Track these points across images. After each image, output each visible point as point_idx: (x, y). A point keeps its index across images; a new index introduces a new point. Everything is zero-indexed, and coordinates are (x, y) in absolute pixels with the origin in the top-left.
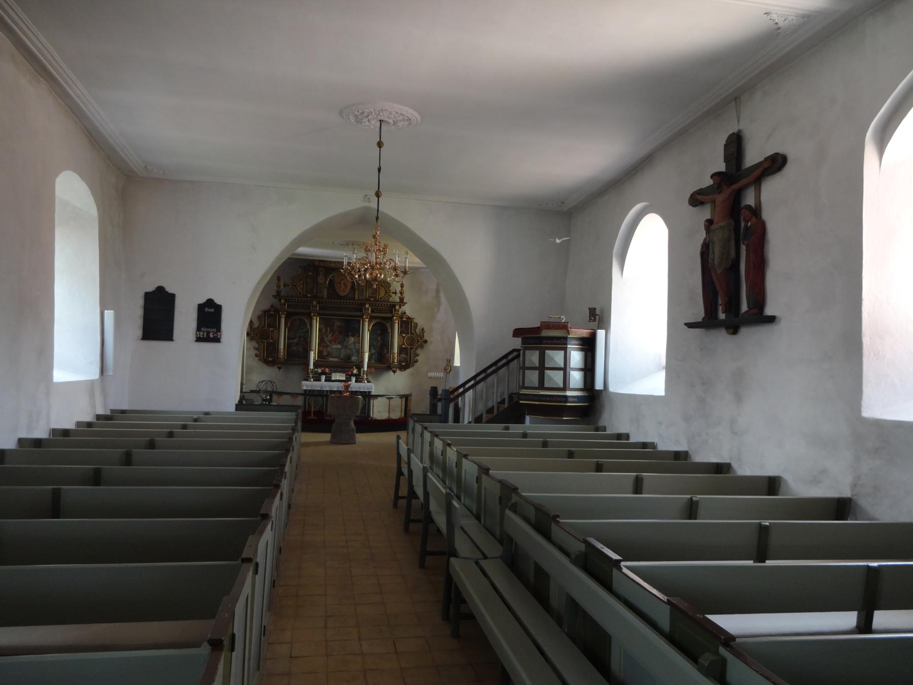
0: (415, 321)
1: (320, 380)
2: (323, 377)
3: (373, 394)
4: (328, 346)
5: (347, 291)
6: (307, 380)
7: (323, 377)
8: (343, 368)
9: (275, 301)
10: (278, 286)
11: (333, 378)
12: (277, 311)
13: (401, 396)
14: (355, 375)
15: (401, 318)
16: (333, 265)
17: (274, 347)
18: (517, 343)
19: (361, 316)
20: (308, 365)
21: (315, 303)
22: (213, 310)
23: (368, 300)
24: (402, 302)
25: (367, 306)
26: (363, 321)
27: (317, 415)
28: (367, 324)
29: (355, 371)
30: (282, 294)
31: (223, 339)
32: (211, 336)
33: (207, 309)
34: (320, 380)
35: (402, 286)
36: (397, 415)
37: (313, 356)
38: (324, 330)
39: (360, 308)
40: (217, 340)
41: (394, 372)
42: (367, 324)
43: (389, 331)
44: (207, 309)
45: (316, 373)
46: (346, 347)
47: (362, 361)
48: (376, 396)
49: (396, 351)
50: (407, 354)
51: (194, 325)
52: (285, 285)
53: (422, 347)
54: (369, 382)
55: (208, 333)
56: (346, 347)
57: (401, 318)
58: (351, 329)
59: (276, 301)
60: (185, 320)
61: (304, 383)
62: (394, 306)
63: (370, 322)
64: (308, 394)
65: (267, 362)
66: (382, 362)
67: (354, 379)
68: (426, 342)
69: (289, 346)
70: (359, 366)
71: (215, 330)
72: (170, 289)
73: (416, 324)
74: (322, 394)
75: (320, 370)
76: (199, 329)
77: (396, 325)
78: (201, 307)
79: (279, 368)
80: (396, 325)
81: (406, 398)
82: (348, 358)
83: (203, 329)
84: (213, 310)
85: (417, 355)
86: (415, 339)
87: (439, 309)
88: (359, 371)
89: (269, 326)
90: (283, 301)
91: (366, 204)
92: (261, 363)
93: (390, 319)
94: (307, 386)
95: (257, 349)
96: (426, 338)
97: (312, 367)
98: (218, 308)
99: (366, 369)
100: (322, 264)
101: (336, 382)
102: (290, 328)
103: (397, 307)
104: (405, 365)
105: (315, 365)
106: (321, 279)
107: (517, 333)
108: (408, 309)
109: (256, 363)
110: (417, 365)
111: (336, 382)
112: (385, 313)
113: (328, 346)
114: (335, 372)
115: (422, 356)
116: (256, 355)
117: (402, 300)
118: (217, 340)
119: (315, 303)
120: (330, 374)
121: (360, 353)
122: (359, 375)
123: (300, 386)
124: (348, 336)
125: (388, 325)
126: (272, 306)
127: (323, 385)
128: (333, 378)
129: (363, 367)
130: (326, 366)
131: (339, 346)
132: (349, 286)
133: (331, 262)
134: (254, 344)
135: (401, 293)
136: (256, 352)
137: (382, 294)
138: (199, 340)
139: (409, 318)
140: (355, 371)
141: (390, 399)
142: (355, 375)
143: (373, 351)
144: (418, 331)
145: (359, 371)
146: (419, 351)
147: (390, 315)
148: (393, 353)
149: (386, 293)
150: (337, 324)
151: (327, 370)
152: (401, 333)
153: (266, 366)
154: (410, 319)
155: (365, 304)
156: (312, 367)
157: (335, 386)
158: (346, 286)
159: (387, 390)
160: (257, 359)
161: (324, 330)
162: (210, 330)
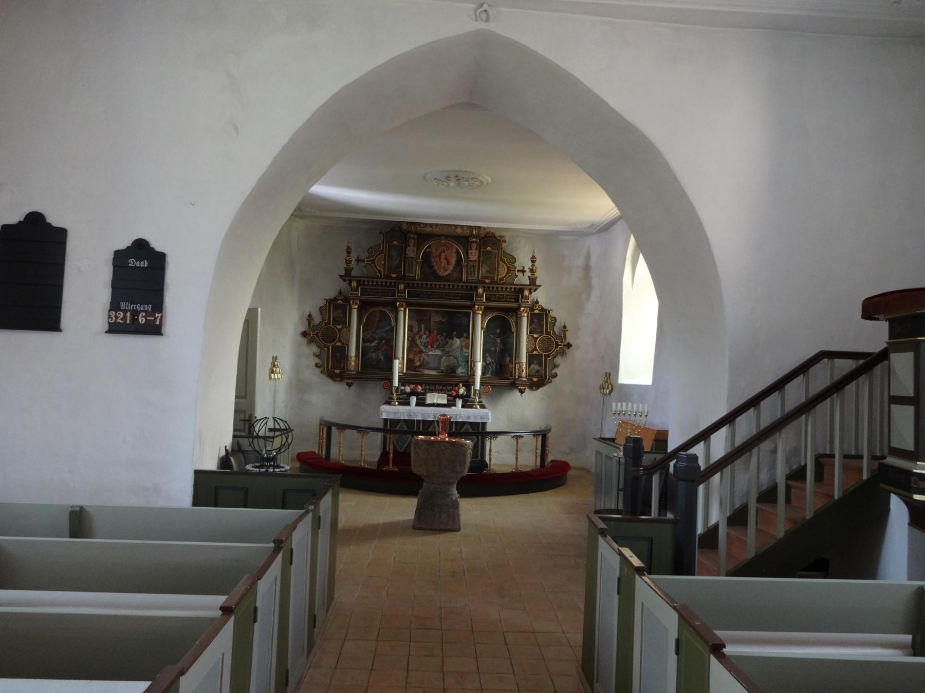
0: (552, 314)
1: (408, 404)
2: (414, 400)
3: (489, 428)
4: (421, 352)
5: (451, 268)
6: (388, 403)
7: (414, 400)
8: (444, 385)
9: (343, 285)
10: (348, 262)
11: (428, 401)
12: (347, 300)
13: (535, 434)
14: (462, 397)
15: (532, 309)
16: (428, 229)
17: (340, 354)
18: (875, 336)
19: (472, 307)
20: (391, 380)
21: (401, 287)
22: (145, 264)
23: (479, 282)
24: (533, 285)
25: (480, 291)
26: (475, 314)
27: (398, 467)
28: (479, 318)
29: (462, 391)
30: (354, 273)
31: (169, 326)
32: (142, 320)
33: (132, 262)
34: (408, 404)
35: (533, 260)
36: (528, 460)
37: (397, 366)
38: (416, 329)
39: (470, 294)
40: (154, 330)
41: (522, 392)
42: (479, 318)
43: (514, 329)
44: (132, 262)
45: (403, 392)
46: (448, 354)
47: (473, 375)
48: (495, 434)
49: (524, 359)
50: (540, 364)
51: (105, 295)
52: (358, 261)
53: (563, 353)
54: (483, 407)
55: (135, 314)
56: (448, 354)
57: (532, 309)
58: (458, 327)
59: (346, 284)
60: (87, 286)
61: (385, 408)
62: (521, 291)
63: (487, 310)
64: (391, 427)
65: (332, 376)
66: (502, 376)
67: (459, 403)
68: (569, 346)
69: (364, 353)
70: (468, 384)
71: (149, 308)
72: (55, 220)
73: (555, 320)
74: (412, 427)
75: (408, 389)
76: (114, 306)
77: (525, 319)
78: (120, 258)
79: (349, 385)
80: (525, 319)
81: (543, 435)
82: (452, 369)
83: (123, 305)
84: (145, 264)
85: (556, 366)
86: (553, 343)
87: (588, 298)
88: (468, 389)
89: (336, 322)
90: (354, 284)
91: (481, 25)
92: (323, 376)
93: (515, 311)
94: (388, 413)
95: (318, 356)
96: (570, 339)
97: (396, 383)
98: (158, 261)
99: (478, 386)
100: (413, 228)
101: (435, 407)
102: (366, 326)
103: (526, 293)
104: (538, 381)
105: (402, 381)
106: (411, 252)
107: (873, 308)
108: (541, 297)
109: (314, 376)
110: (555, 380)
111: (435, 407)
112: (508, 305)
113: (421, 352)
114: (432, 391)
115: (564, 367)
116: (317, 365)
117: (533, 281)
118: (154, 330)
119: (401, 287)
120: (425, 394)
121: (470, 363)
122: (468, 396)
123: (378, 412)
124: (452, 338)
125: (512, 321)
126: (340, 293)
127: (413, 411)
128: (428, 401)
129: (473, 383)
130: (419, 383)
131: (438, 353)
132: (453, 261)
133: (426, 225)
134: (314, 349)
135: (532, 271)
136: (317, 360)
137: (503, 272)
138: (114, 329)
139: (543, 310)
140: (462, 391)
141: (517, 437)
142: (462, 397)
143: (489, 360)
144: (556, 329)
145: (468, 389)
146: (558, 360)
147: (514, 305)
148: (520, 364)
149: (509, 270)
150: (436, 319)
151: (419, 388)
152: (531, 332)
153: (330, 381)
154: (544, 312)
155: (476, 288)
156: (396, 383)
157: (429, 414)
158: (448, 262)
159: (511, 420)
160: (318, 370)
161: (416, 329)
162: (139, 307)
